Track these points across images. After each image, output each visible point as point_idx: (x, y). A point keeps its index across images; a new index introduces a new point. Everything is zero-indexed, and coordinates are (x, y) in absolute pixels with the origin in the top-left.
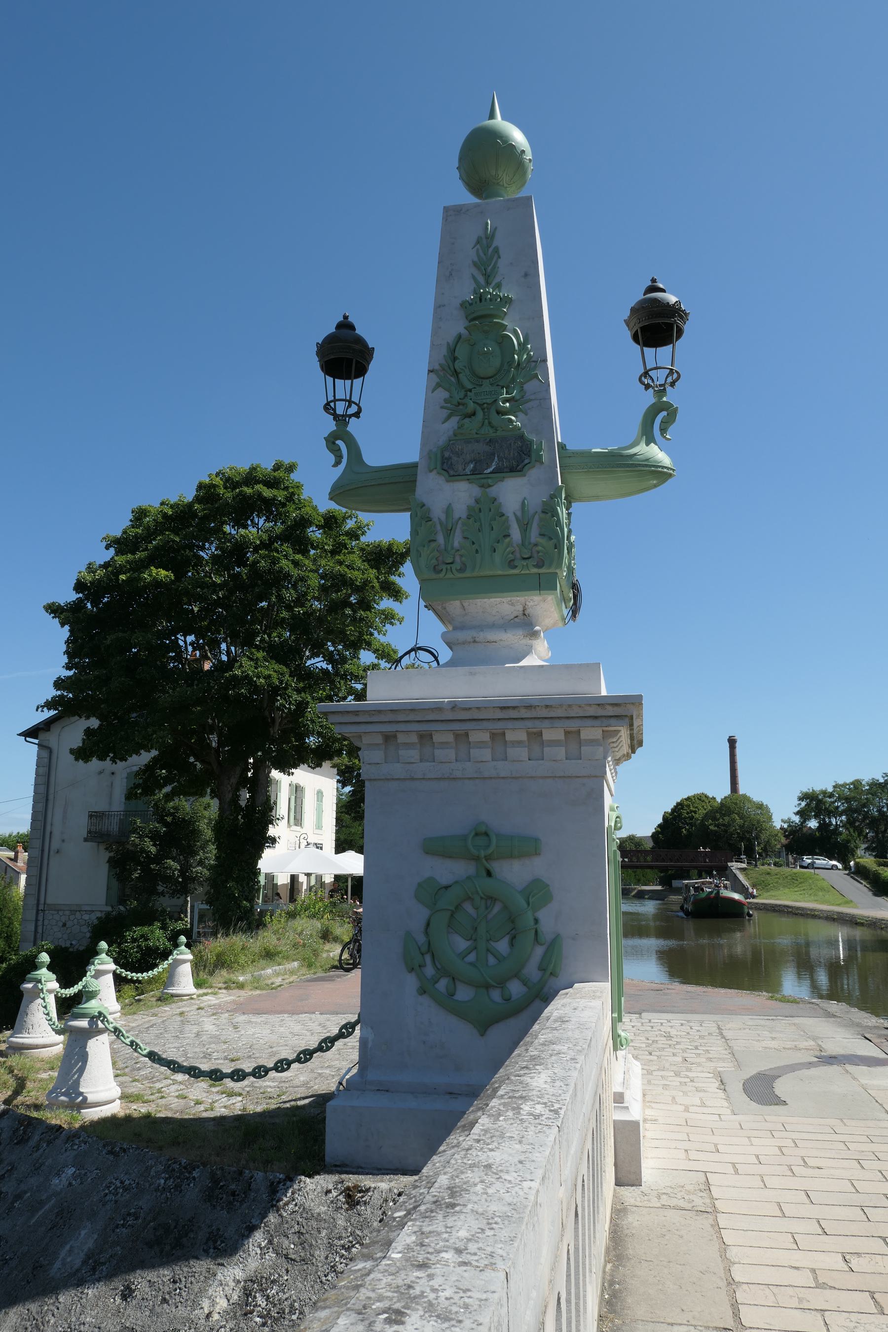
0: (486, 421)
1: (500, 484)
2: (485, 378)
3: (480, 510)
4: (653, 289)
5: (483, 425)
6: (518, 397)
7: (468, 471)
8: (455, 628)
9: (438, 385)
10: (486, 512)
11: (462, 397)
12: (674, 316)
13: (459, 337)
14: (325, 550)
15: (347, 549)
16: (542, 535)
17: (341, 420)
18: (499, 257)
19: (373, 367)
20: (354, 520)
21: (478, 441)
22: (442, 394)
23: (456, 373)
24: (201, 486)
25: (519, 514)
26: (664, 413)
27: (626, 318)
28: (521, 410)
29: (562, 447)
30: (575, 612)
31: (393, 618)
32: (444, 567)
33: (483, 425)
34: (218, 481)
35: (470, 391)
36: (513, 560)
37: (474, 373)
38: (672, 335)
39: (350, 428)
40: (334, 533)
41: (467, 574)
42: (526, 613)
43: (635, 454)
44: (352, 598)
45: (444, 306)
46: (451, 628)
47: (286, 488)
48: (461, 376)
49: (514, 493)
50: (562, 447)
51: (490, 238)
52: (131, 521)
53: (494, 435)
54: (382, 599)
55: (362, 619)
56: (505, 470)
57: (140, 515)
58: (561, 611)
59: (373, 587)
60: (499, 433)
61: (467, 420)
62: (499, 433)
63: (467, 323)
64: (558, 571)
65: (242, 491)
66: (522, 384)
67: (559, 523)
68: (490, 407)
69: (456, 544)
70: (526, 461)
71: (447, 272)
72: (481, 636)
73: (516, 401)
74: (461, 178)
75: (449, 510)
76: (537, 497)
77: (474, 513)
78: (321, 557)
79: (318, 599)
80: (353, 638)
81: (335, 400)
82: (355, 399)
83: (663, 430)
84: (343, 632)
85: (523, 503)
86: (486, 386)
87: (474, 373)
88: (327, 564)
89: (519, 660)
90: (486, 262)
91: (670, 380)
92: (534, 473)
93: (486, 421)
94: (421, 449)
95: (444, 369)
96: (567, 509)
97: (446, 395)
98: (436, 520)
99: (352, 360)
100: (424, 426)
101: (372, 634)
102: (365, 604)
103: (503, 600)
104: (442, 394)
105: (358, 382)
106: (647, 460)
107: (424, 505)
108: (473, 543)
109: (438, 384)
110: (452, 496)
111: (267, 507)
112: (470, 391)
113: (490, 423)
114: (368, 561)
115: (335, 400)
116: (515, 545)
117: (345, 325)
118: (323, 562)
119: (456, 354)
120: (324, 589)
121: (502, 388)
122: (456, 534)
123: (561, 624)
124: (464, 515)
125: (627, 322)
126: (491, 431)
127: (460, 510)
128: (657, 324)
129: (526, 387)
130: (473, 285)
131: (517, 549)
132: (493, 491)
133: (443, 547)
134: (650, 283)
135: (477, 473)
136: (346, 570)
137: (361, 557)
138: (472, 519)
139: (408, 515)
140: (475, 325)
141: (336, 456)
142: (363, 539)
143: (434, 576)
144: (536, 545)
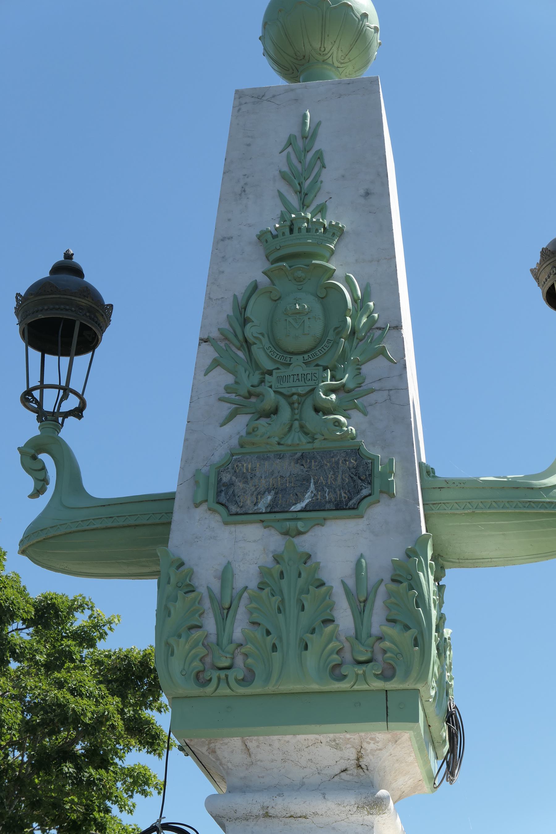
0: (296, 424)
1: (318, 530)
2: (298, 367)
6: (351, 386)
7: (262, 506)
8: (231, 790)
9: (216, 363)
10: (292, 581)
11: (256, 382)
13: (255, 287)
14: (37, 663)
15: (73, 661)
16: (391, 621)
17: (51, 420)
18: (324, 167)
19: (109, 338)
20: (88, 612)
21: (280, 456)
22: (222, 378)
23: (247, 344)
25: (351, 583)
27: (534, 266)
28: (356, 407)
30: (452, 762)
31: (146, 783)
32: (215, 674)
35: (270, 373)
36: (339, 665)
37: (277, 345)
39: (63, 434)
40: (52, 633)
41: (255, 689)
42: (363, 764)
44: (78, 747)
45: (230, 238)
46: (225, 790)
48: (254, 348)
49: (340, 547)
50: (427, 472)
51: (309, 138)
53: (310, 446)
54: (129, 750)
55: (91, 783)
56: (328, 506)
58: (426, 762)
59: (113, 727)
60: (317, 444)
61: (263, 421)
62: (317, 444)
63: (267, 266)
64: (419, 686)
66: (358, 365)
67: (421, 601)
68: (303, 400)
69: (238, 635)
70: (365, 492)
71: (237, 187)
72: (280, 805)
73: (349, 391)
74: (266, 53)
75: (226, 574)
76: (382, 556)
77: (271, 580)
78: (28, 673)
79: (21, 747)
80: (74, 816)
81: (42, 387)
82: (76, 384)
84: (57, 805)
85: (358, 564)
86: (298, 366)
87: (277, 345)
88: (38, 686)
90: (303, 169)
92: (378, 512)
93: (296, 424)
94: (182, 468)
95: (226, 338)
96: (437, 579)
97: (230, 379)
98: (203, 590)
99: (74, 322)
100: (189, 430)
101: (107, 811)
102: (100, 759)
103: (321, 737)
104: (222, 378)
105: (81, 361)
107: (182, 564)
108: (268, 633)
110: (230, 550)
112: (270, 373)
113: (302, 427)
114: (107, 682)
115: (42, 387)
116: (343, 638)
117: (67, 268)
118: (30, 682)
119: (248, 314)
120: (28, 728)
121: (325, 369)
122: (238, 617)
123: (426, 787)
124: (253, 584)
125: (536, 274)
126: (304, 439)
127: (247, 575)
129: (366, 369)
130: (280, 208)
131: (347, 645)
132: (304, 543)
133: (213, 638)
136: (69, 696)
137: (95, 676)
138: (267, 590)
139: (152, 584)
140: (281, 269)
141: (36, 479)
142: (101, 645)
143: (196, 691)
144: (380, 639)
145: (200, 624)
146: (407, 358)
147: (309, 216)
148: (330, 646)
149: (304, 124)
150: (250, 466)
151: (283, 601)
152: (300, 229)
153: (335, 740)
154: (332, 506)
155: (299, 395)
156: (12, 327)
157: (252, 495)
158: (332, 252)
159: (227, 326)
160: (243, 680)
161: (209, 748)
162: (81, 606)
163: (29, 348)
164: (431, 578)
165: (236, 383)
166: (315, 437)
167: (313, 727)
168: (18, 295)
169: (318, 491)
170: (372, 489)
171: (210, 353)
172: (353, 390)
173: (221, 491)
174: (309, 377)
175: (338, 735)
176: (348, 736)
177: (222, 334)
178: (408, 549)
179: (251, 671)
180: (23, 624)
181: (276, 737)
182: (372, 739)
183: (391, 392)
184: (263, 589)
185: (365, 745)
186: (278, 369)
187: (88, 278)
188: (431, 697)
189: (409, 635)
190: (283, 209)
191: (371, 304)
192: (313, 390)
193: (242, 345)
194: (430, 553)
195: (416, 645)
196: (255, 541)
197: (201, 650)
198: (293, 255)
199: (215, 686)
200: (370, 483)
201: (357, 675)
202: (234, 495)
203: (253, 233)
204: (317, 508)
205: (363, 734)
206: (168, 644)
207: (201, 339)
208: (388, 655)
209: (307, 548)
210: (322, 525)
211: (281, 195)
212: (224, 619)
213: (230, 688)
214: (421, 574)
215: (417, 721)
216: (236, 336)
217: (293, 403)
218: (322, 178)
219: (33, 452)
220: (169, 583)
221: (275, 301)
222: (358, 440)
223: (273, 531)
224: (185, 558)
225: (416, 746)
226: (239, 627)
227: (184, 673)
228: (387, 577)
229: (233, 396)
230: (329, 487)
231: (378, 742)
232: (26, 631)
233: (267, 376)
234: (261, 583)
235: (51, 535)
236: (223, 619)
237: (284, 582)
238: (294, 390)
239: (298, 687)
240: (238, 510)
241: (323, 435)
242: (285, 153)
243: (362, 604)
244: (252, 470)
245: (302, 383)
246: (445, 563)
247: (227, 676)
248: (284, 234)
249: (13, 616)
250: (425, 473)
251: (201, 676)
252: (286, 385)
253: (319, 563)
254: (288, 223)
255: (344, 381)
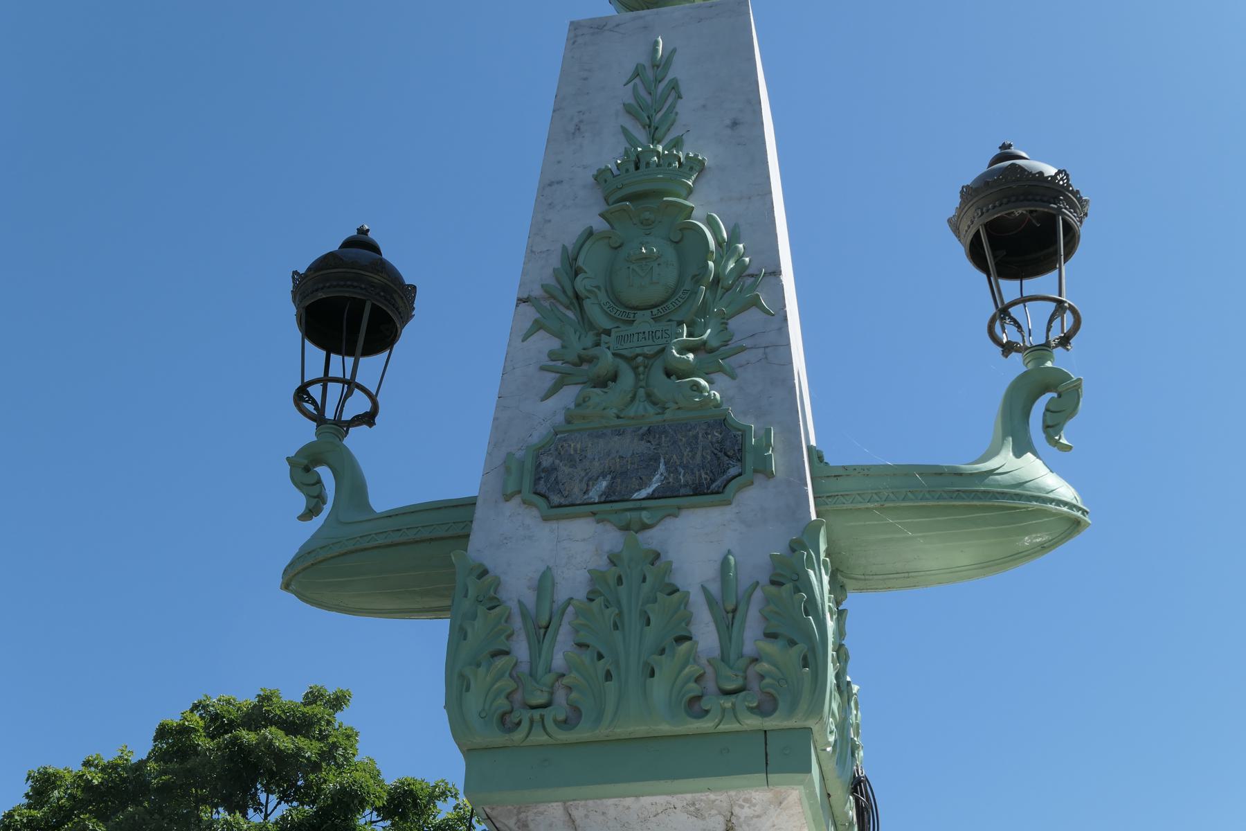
0: (641, 392)
1: (670, 523)
3: (620, 581)
5: (633, 398)
7: (594, 495)
9: (537, 326)
10: (635, 592)
12: (1056, 200)
13: (590, 233)
16: (771, 636)
18: (680, 97)
21: (620, 432)
22: (545, 343)
24: (163, 732)
25: (714, 588)
27: (951, 212)
28: (721, 369)
29: (816, 456)
32: (526, 715)
33: (633, 398)
34: (196, 720)
35: (608, 332)
36: (698, 698)
37: (617, 300)
38: (1057, 252)
43: (991, 472)
45: (560, 182)
47: (323, 738)
48: (587, 304)
49: (701, 543)
50: (816, 456)
51: (661, 66)
52: (27, 796)
53: (659, 418)
56: (683, 491)
57: (43, 784)
60: (668, 415)
63: (603, 207)
64: (810, 723)
65: (236, 738)
66: (724, 321)
67: (812, 606)
69: (558, 661)
70: (733, 471)
71: (570, 124)
73: (712, 351)
75: (545, 583)
77: (604, 588)
83: (1051, 429)
85: (725, 563)
86: (644, 322)
87: (617, 300)
91: (1055, 334)
92: (752, 498)
93: (641, 392)
94: (489, 454)
95: (552, 297)
97: (555, 344)
99: (363, 303)
100: (500, 407)
103: (674, 800)
104: (545, 343)
106: (1021, 485)
107: (485, 572)
108: (600, 657)
109: (536, 321)
111: (282, 772)
112: (608, 332)
116: (704, 661)
119: (580, 262)
121: (680, 324)
122: (559, 638)
124: (581, 594)
125: (955, 225)
126: (651, 410)
127: (572, 582)
128: (1019, 227)
129: (733, 324)
130: (623, 144)
131: (709, 670)
132: (652, 539)
133: (524, 668)
134: (998, 151)
135: (617, 500)
141: (308, 496)
143: (500, 738)
146: (788, 309)
147: (660, 148)
148: (687, 670)
149: (656, 51)
150: (579, 446)
151: (620, 614)
152: (648, 164)
153: (694, 804)
154: (688, 491)
155: (646, 356)
156: (288, 312)
157: (581, 481)
158: (690, 191)
159: (553, 282)
160: (565, 721)
161: (518, 820)
162: (443, 793)
163: (307, 342)
164: (826, 579)
165: (563, 347)
167: (663, 785)
168: (295, 273)
169: (669, 472)
170: (743, 467)
171: (530, 313)
172: (718, 348)
173: (540, 478)
174: (659, 334)
175: (697, 795)
176: (712, 796)
177: (546, 291)
178: (792, 541)
179: (576, 710)
180: (378, 815)
181: (611, 801)
182: (746, 800)
183: (768, 350)
184: (591, 600)
185: (736, 810)
187: (387, 255)
188: (828, 744)
189: (796, 652)
190: (628, 146)
191: (741, 246)
192: (663, 350)
193: (572, 303)
194: (823, 547)
195: (805, 666)
196: (584, 540)
197: (506, 684)
198: (640, 196)
199: (527, 730)
200: (739, 460)
201: (724, 710)
202: (557, 482)
203: (588, 176)
204: (668, 494)
205: (733, 793)
206: (462, 676)
207: (519, 299)
208: (767, 681)
209: (654, 545)
210: (676, 516)
211: (625, 131)
212: (540, 642)
213: (547, 734)
214: (811, 572)
215: (809, 770)
216: (564, 292)
217: (637, 367)
218: (678, 109)
219: (306, 462)
220: (466, 596)
222: (724, 407)
223: (609, 526)
224: (488, 564)
225: (809, 813)
226: (561, 652)
227: (483, 715)
228: (764, 579)
229: (559, 363)
230: (685, 467)
231: (754, 805)
232: (381, 823)
234: (592, 592)
235: (321, 558)
237: (622, 589)
238: (638, 351)
239: (641, 730)
240: (563, 501)
242: (631, 84)
243: (730, 615)
244: (582, 450)
245: (650, 342)
246: (845, 581)
247: (542, 717)
248: (627, 171)
249: (362, 803)
250: (816, 459)
251: (507, 718)
252: (627, 345)
253: (670, 563)
254: (633, 158)
255: (705, 336)
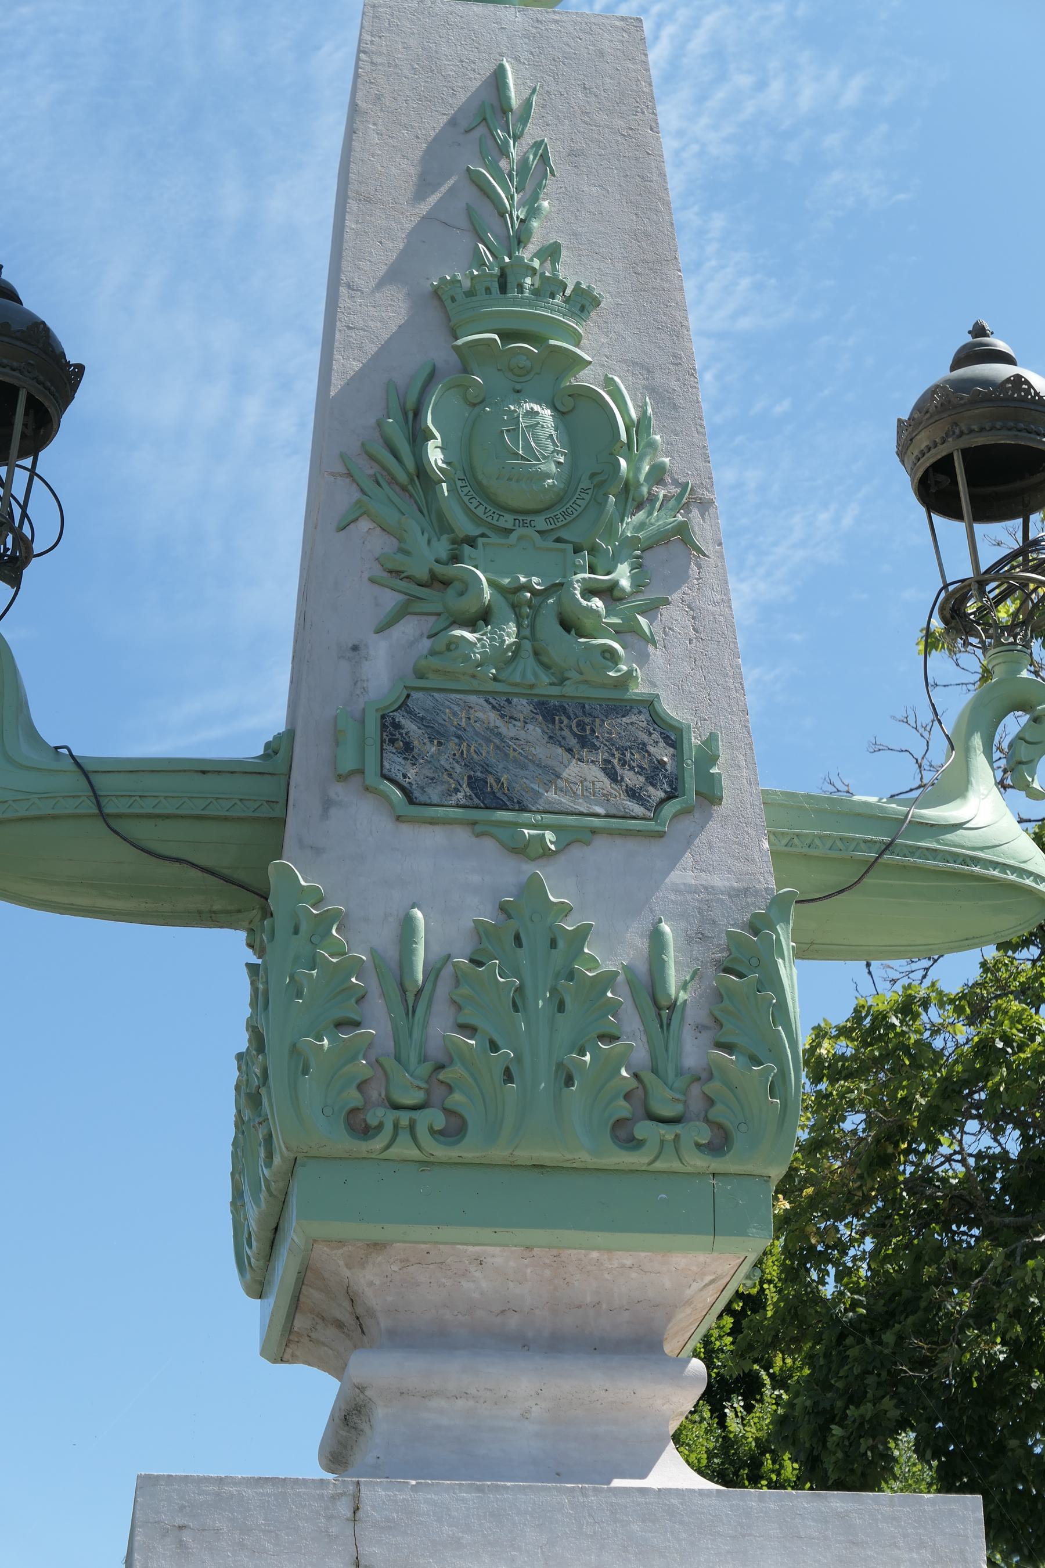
4: (978, 352)
9: (359, 512)
11: (444, 555)
26: (1013, 724)
35: (471, 542)
41: (466, 1151)
62: (569, 690)
89: (643, 1476)
112: (471, 542)
121: (577, 550)
126: (545, 678)
134: (969, 339)
143: (345, 1143)
145: (357, 1018)
166: (567, 675)
186: (483, 535)
210: (588, 844)
214: (780, 961)
221: (474, 405)
233: (467, 548)
236: (407, 1014)
241: (581, 673)
